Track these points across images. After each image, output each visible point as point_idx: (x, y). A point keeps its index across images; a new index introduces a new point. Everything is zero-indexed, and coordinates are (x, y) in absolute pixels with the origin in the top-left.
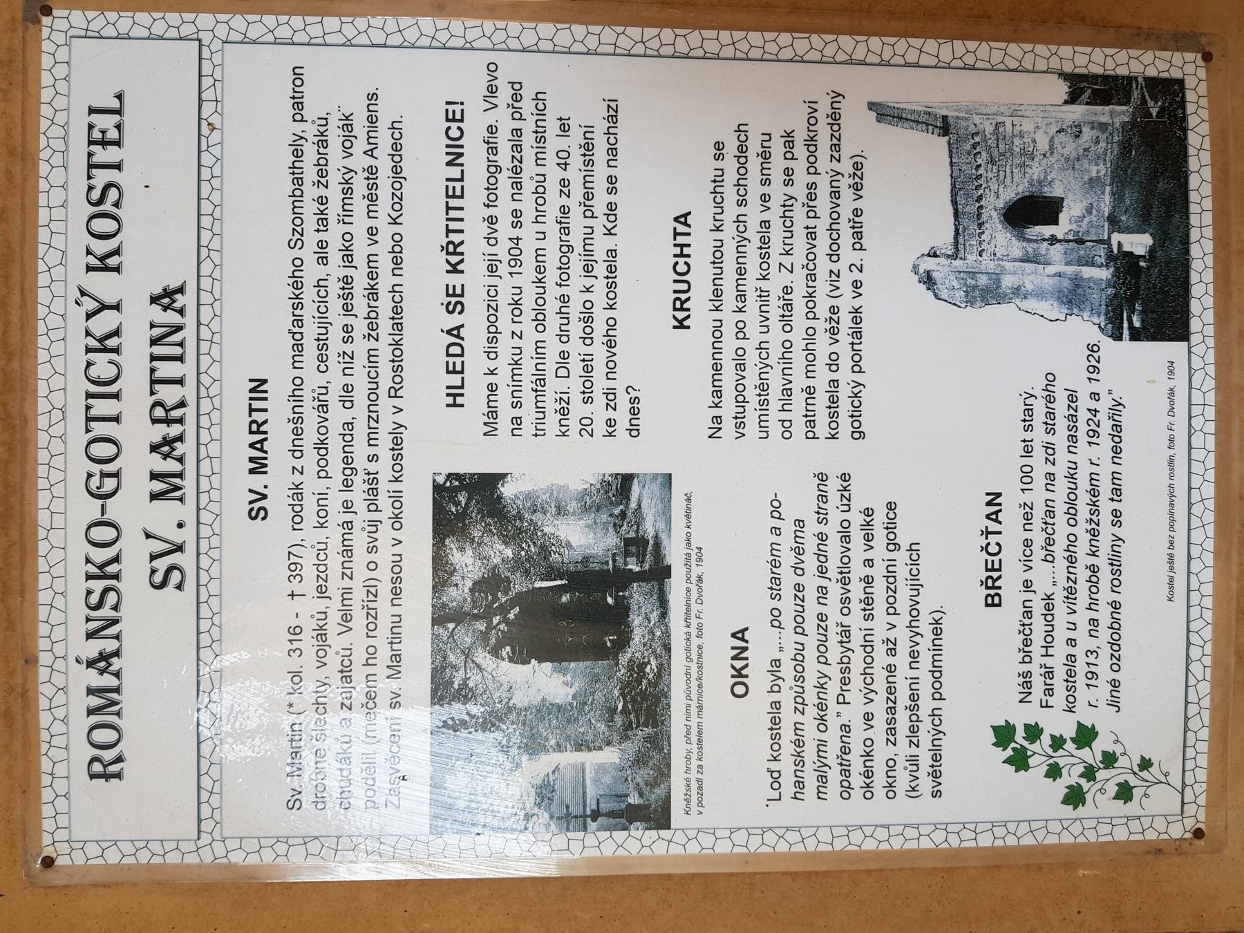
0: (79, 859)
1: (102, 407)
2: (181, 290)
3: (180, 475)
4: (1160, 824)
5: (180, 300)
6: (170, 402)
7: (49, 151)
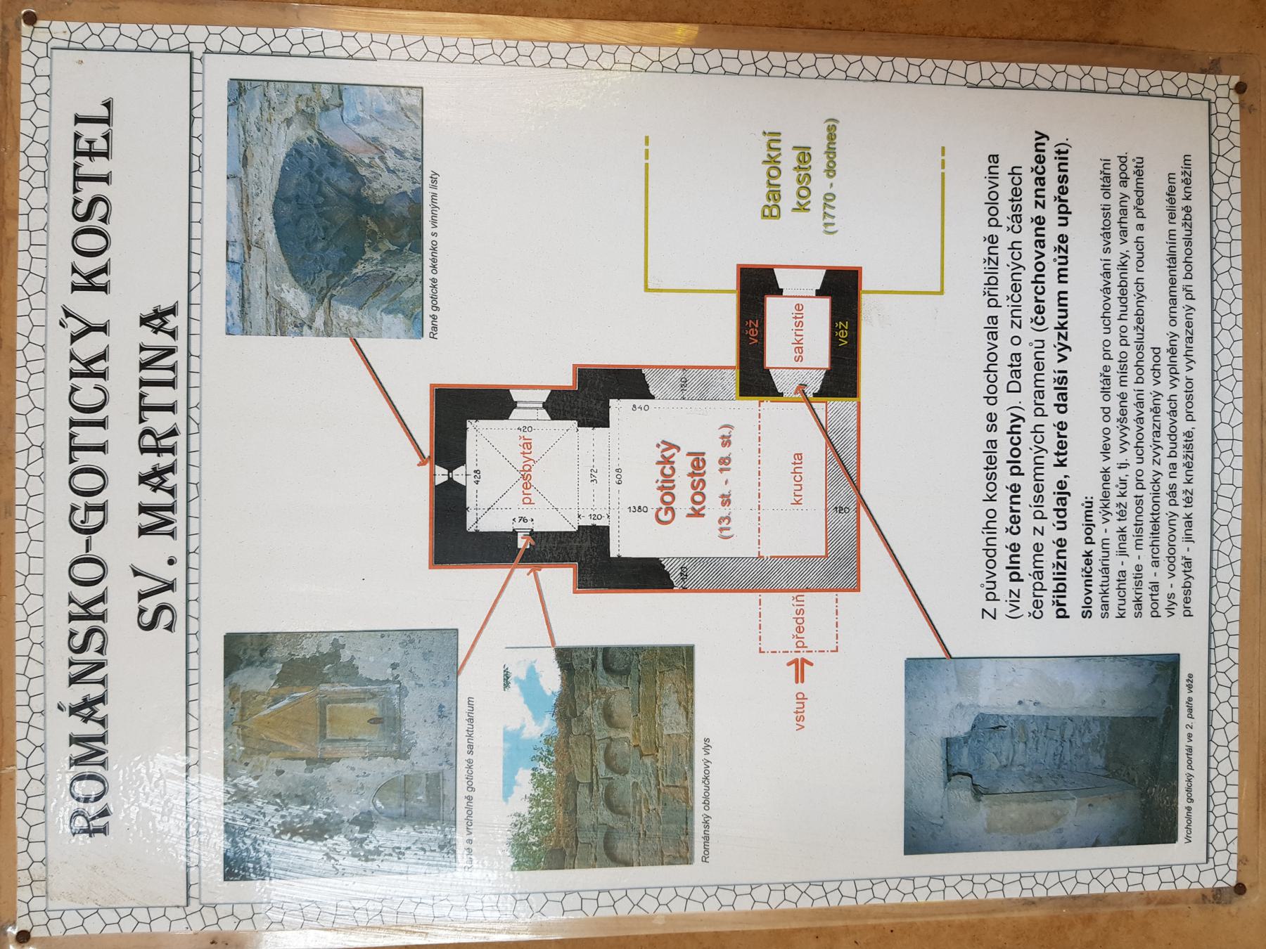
0: (57, 930)
1: (87, 436)
2: (173, 311)
3: (171, 508)
4: (1192, 873)
5: (172, 322)
6: (161, 429)
7: (29, 171)
